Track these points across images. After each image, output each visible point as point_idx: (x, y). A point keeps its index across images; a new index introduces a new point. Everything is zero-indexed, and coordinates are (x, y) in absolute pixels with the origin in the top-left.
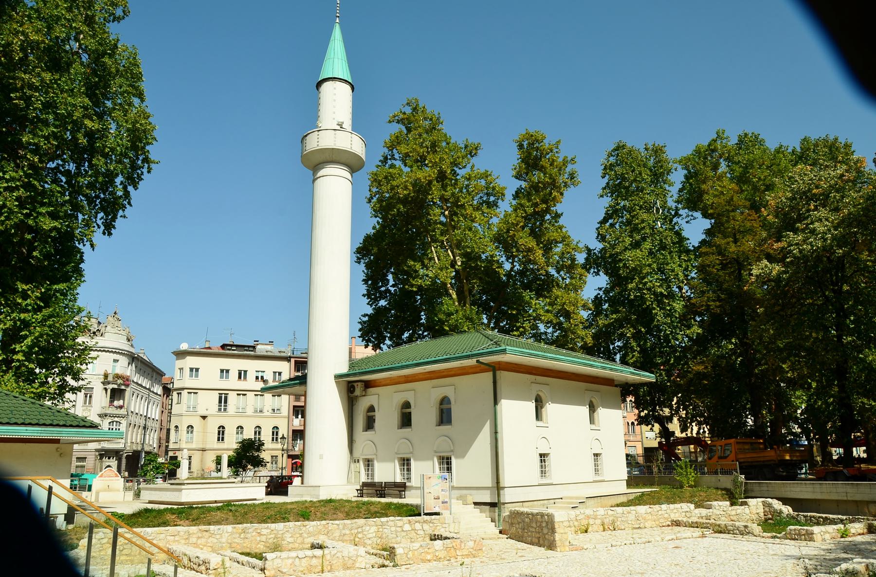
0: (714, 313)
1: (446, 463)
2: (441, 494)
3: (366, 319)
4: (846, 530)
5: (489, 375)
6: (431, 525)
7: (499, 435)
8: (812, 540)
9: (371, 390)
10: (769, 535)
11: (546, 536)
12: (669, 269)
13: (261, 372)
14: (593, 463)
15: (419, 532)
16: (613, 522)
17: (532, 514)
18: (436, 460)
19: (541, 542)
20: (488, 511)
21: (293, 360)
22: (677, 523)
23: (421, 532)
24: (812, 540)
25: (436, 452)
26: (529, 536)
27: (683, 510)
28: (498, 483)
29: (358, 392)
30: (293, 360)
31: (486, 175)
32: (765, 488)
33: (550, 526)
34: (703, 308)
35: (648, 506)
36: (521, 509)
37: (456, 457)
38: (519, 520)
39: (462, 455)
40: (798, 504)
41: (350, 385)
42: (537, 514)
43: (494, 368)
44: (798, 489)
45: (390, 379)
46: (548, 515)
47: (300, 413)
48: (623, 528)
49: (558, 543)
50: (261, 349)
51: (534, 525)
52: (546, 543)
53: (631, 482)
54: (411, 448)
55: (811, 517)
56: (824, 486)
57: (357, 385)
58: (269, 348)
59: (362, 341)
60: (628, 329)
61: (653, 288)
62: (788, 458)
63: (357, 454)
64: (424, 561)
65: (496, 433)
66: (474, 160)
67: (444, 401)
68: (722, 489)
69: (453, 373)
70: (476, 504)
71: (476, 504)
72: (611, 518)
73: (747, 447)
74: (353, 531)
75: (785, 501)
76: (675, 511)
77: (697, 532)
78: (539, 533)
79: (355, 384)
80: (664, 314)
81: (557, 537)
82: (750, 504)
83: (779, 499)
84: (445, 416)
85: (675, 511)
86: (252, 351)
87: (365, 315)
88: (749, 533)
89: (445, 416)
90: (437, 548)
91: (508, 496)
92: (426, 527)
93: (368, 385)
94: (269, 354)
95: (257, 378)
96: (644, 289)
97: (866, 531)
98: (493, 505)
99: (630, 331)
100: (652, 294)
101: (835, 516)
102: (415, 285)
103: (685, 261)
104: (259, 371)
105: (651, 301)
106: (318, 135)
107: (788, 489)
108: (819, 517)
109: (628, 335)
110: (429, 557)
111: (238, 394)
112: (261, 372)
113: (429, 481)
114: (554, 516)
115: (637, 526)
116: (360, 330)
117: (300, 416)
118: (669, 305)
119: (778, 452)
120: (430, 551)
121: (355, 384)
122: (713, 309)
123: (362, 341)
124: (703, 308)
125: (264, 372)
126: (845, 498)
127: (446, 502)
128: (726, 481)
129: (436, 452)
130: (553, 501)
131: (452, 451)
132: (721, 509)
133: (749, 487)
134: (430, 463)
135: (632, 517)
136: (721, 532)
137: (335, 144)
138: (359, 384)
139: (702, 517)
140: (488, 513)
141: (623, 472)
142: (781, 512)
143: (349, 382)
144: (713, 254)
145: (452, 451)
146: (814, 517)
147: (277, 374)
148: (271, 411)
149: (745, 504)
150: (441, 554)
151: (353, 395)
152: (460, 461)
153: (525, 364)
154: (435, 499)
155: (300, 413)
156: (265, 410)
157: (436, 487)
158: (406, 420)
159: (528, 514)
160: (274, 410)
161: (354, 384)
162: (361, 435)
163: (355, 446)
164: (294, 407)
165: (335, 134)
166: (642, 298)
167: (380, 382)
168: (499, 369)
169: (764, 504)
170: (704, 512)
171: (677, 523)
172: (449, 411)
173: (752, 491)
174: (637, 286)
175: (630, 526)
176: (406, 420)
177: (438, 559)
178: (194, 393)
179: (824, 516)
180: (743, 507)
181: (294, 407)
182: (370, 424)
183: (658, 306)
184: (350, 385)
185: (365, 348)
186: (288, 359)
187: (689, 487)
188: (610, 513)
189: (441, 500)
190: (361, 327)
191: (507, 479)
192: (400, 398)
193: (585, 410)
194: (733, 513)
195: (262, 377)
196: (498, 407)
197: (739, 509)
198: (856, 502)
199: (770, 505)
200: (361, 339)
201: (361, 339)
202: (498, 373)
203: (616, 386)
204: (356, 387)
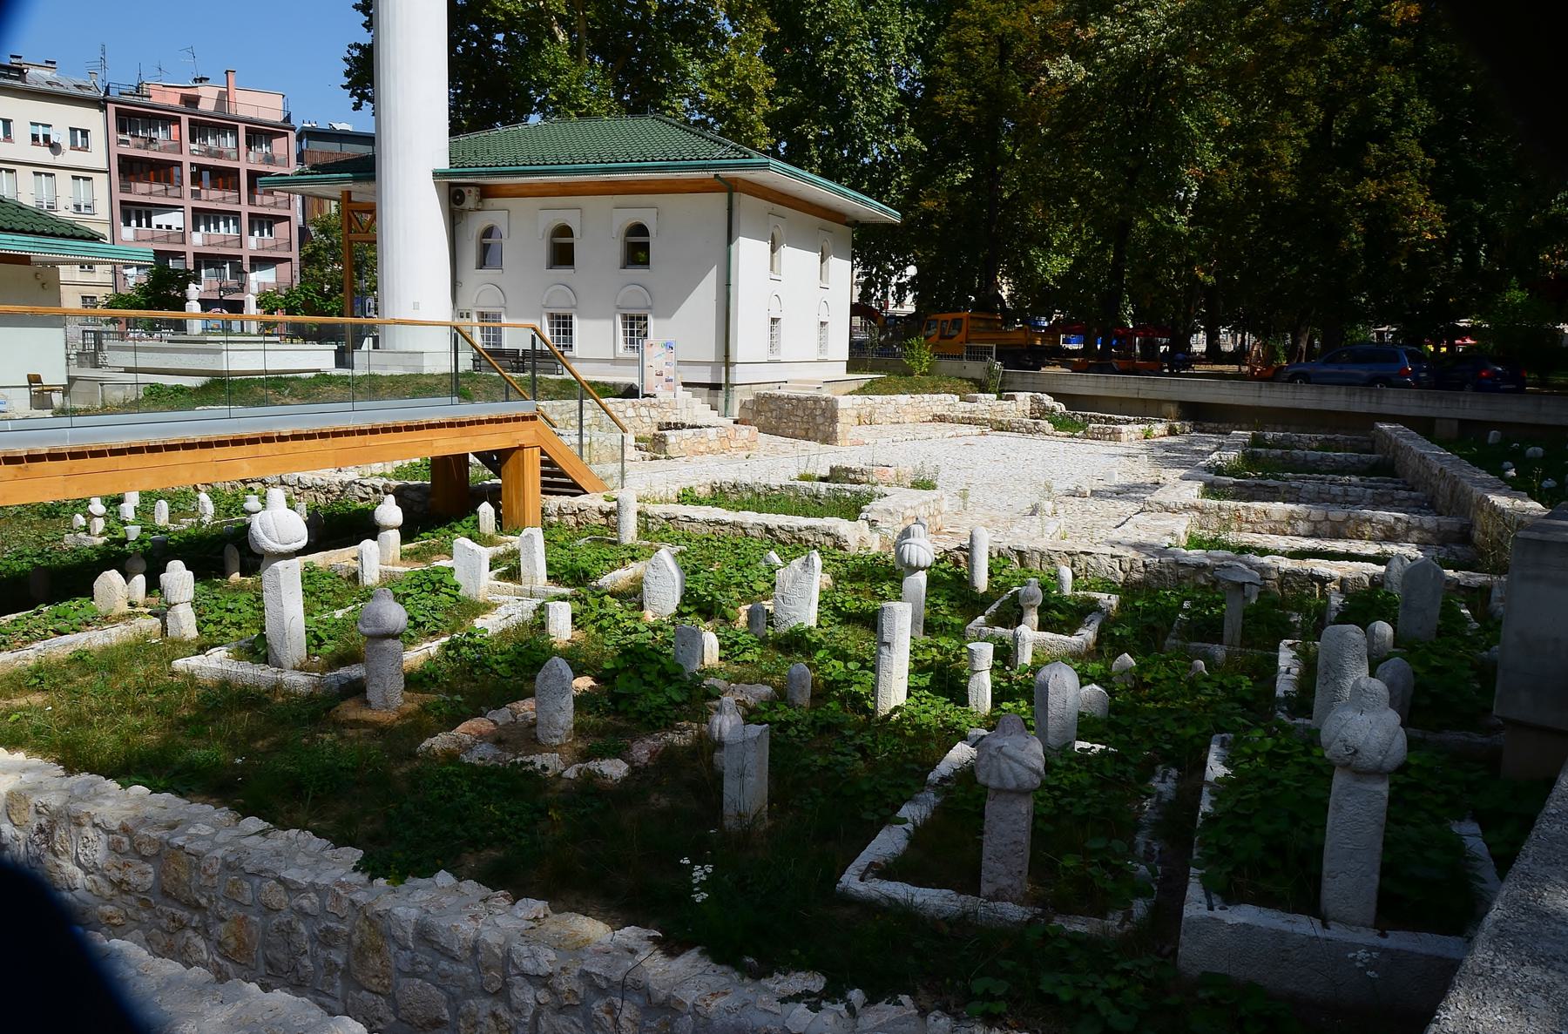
0: (966, 123)
1: (635, 326)
2: (665, 369)
3: (356, 53)
4: (1150, 431)
5: (723, 197)
6: (660, 410)
7: (732, 289)
8: (1118, 439)
10: (1064, 434)
11: (821, 427)
12: (887, 34)
13: (44, 125)
15: (645, 419)
16: (871, 414)
17: (798, 399)
18: (619, 319)
19: (811, 434)
20: (706, 395)
21: (111, 108)
22: (941, 419)
23: (647, 420)
24: (1118, 439)
25: (618, 307)
26: (789, 427)
27: (945, 402)
28: (727, 356)
29: (470, 201)
30: (111, 108)
32: (1030, 380)
33: (828, 414)
34: (951, 112)
35: (908, 396)
36: (778, 392)
37: (656, 317)
38: (772, 407)
39: (667, 313)
40: (1071, 401)
42: (807, 399)
43: (731, 188)
44: (1076, 383)
45: (530, 185)
46: (826, 400)
47: (133, 216)
49: (840, 436)
50: (38, 76)
51: (800, 413)
52: (819, 435)
53: (852, 366)
54: (573, 299)
55: (1090, 417)
56: (1112, 380)
58: (47, 74)
59: (351, 96)
60: (809, 127)
61: (860, 62)
62: (1039, 343)
63: (464, 305)
65: (728, 285)
67: (639, 229)
68: (968, 380)
69: (653, 187)
70: (685, 384)
71: (685, 384)
72: (869, 409)
73: (981, 325)
74: (563, 416)
75: (1058, 397)
76: (938, 403)
77: (976, 430)
78: (808, 422)
79: (466, 190)
80: (868, 108)
81: (839, 427)
82: (1018, 398)
83: (1049, 394)
84: (637, 250)
85: (938, 403)
86: (16, 79)
87: (357, 46)
88: (1038, 431)
89: (637, 250)
90: (710, 437)
91: (740, 375)
92: (653, 412)
93: (486, 192)
94: (56, 88)
95: (35, 138)
96: (845, 63)
97: (1166, 433)
98: (715, 387)
99: (813, 130)
100: (856, 74)
101: (1120, 417)
102: (501, 9)
103: (911, 23)
104: (37, 124)
105: (854, 85)
107: (1063, 382)
108: (1101, 417)
109: (810, 137)
110: (702, 448)
111: (36, 174)
112: (44, 125)
113: (650, 349)
114: (837, 402)
116: (347, 74)
117: (134, 223)
118: (879, 95)
119: (1029, 335)
120: (703, 441)
121: (466, 190)
122: (965, 116)
123: (351, 96)
124: (951, 112)
125: (49, 126)
126: (1136, 396)
127: (671, 380)
128: (975, 369)
129: (618, 307)
130: (778, 384)
131: (649, 308)
132: (987, 403)
133: (1007, 377)
134: (608, 324)
135: (891, 408)
136: (1002, 430)
138: (473, 189)
140: (706, 398)
141: (844, 353)
142: (1053, 410)
143: (451, 185)
144: (974, 24)
145: (649, 308)
146: (1094, 417)
147: (79, 132)
148: (72, 208)
149: (1013, 398)
150: (715, 445)
151: (460, 207)
152: (663, 323)
153: (769, 186)
155: (133, 216)
156: (60, 206)
157: (658, 359)
158: (562, 254)
159: (789, 399)
160: (78, 207)
162: (474, 277)
163: (460, 291)
164: (122, 203)
166: (840, 79)
167: (510, 190)
169: (1033, 399)
170: (968, 406)
171: (941, 419)
172: (645, 247)
173: (1011, 383)
174: (836, 55)
175: (888, 419)
176: (562, 254)
177: (712, 452)
178: (8, 171)
179: (1107, 416)
180: (1009, 402)
181: (122, 203)
182: (486, 256)
183: (861, 95)
185: (354, 109)
186: (101, 104)
187: (922, 374)
188: (868, 402)
189: (664, 377)
190: (348, 67)
191: (740, 352)
192: (558, 217)
193: (816, 257)
194: (999, 409)
195: (47, 138)
196: (733, 247)
197: (1006, 405)
198: (1144, 400)
199: (1040, 401)
200: (349, 92)
201: (349, 92)
202: (735, 195)
203: (847, 224)
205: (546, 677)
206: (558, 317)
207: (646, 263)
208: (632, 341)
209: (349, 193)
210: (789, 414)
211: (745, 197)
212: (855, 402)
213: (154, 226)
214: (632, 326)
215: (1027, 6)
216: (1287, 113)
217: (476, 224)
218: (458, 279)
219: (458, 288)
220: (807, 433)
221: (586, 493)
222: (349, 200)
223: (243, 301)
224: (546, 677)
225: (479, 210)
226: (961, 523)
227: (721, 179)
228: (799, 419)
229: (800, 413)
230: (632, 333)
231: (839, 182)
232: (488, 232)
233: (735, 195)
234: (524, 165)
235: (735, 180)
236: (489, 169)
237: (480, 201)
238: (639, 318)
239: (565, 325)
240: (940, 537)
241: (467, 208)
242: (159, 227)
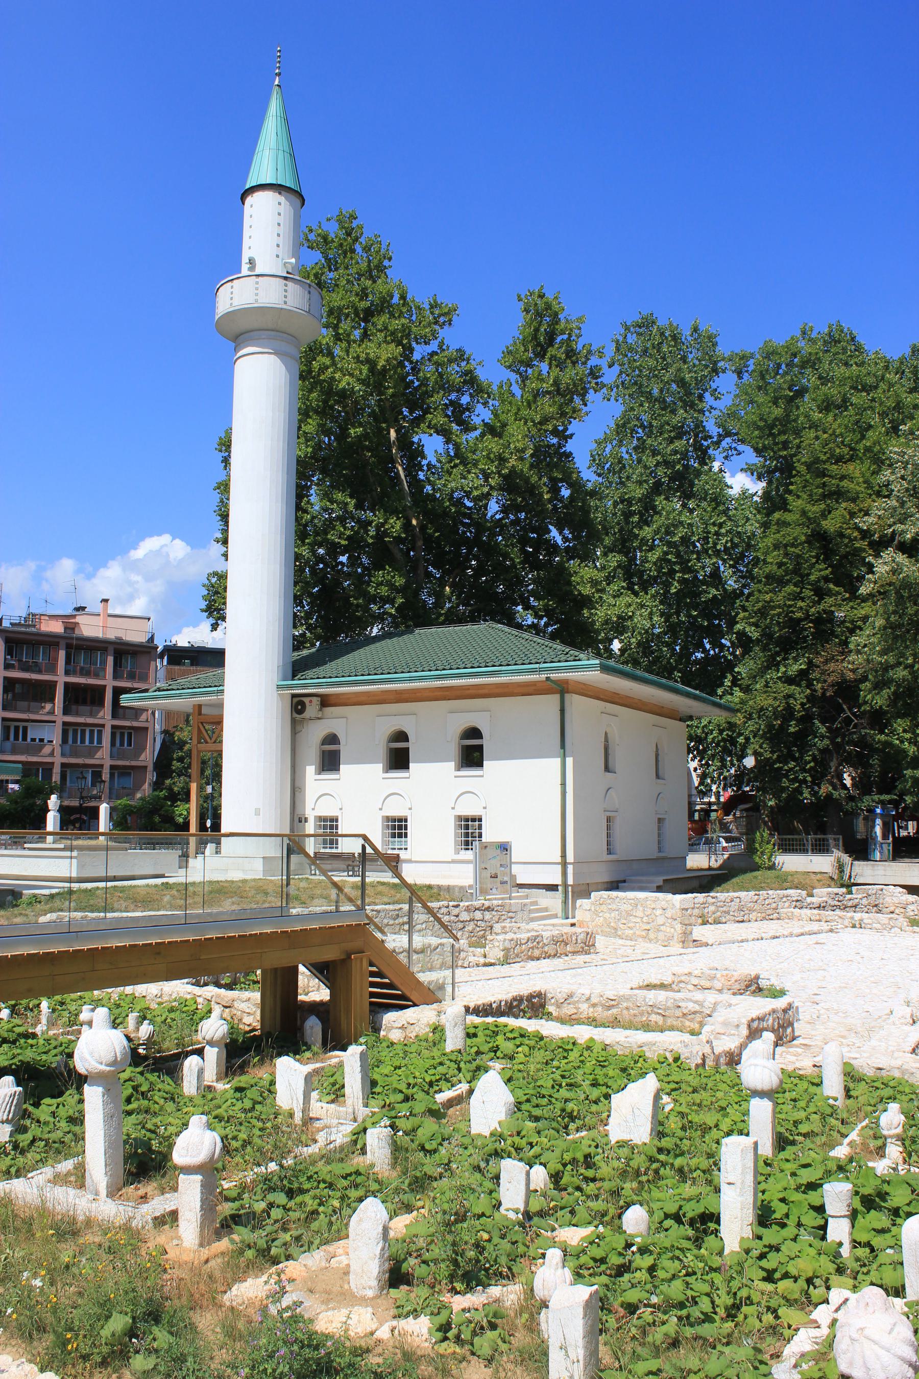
5: (557, 697)
9: (329, 710)
14: (483, 831)
29: (312, 709)
31: (461, 355)
35: (753, 893)
41: (296, 700)
44: (881, 872)
45: (397, 692)
48: (724, 920)
57: (311, 702)
64: (532, 958)
66: (444, 333)
67: (474, 733)
79: (306, 700)
85: (785, 899)
106: (232, 287)
110: (537, 953)
115: (740, 919)
121: (306, 700)
127: (506, 882)
137: (256, 301)
139: (101, 1063)
143: (294, 696)
154: (491, 877)
157: (493, 862)
161: (305, 699)
165: (257, 283)
168: (568, 692)
175: (733, 918)
184: (296, 700)
188: (710, 900)
189: (498, 880)
202: (567, 696)
204: (307, 704)
205: (361, 1220)
206: (394, 820)
207: (479, 764)
208: (467, 843)
209: (200, 706)
210: (629, 914)
211: (576, 697)
212: (696, 901)
213: (29, 740)
214: (467, 827)
215: (463, 942)
216: (737, 689)
217: (315, 733)
218: (297, 784)
219: (297, 793)
220: (648, 934)
221: (415, 1005)
222: (200, 714)
223: (408, 748)
224: (361, 1220)
225: (319, 718)
226: (813, 1033)
227: (552, 681)
228: (638, 920)
229: (640, 913)
230: (467, 835)
231: (669, 678)
232: (332, 739)
233: (567, 696)
234: (363, 675)
235: (566, 682)
236: (329, 680)
237: (321, 710)
238: (474, 820)
239: (400, 827)
240: (791, 1050)
241: (308, 717)
242: (33, 740)
